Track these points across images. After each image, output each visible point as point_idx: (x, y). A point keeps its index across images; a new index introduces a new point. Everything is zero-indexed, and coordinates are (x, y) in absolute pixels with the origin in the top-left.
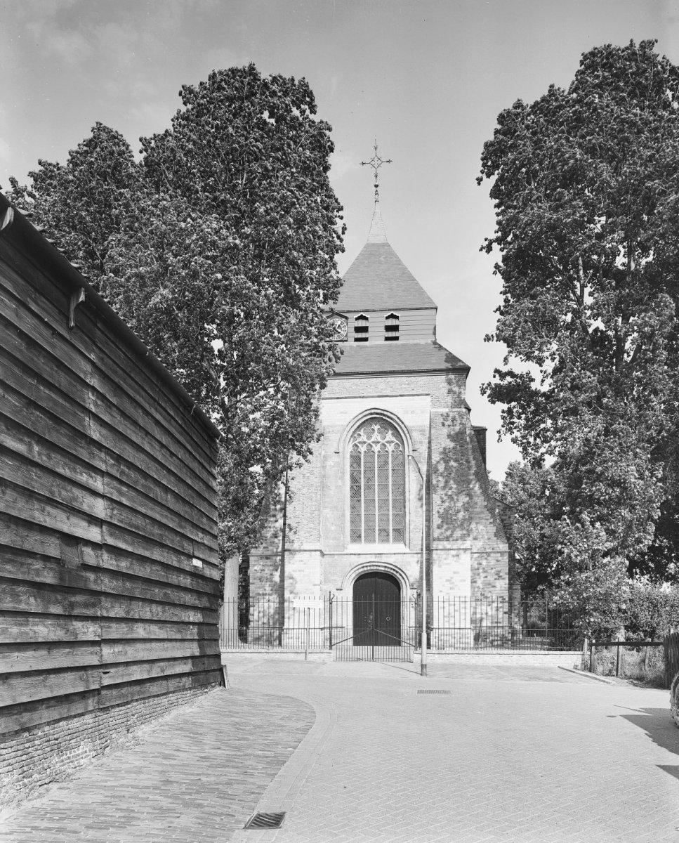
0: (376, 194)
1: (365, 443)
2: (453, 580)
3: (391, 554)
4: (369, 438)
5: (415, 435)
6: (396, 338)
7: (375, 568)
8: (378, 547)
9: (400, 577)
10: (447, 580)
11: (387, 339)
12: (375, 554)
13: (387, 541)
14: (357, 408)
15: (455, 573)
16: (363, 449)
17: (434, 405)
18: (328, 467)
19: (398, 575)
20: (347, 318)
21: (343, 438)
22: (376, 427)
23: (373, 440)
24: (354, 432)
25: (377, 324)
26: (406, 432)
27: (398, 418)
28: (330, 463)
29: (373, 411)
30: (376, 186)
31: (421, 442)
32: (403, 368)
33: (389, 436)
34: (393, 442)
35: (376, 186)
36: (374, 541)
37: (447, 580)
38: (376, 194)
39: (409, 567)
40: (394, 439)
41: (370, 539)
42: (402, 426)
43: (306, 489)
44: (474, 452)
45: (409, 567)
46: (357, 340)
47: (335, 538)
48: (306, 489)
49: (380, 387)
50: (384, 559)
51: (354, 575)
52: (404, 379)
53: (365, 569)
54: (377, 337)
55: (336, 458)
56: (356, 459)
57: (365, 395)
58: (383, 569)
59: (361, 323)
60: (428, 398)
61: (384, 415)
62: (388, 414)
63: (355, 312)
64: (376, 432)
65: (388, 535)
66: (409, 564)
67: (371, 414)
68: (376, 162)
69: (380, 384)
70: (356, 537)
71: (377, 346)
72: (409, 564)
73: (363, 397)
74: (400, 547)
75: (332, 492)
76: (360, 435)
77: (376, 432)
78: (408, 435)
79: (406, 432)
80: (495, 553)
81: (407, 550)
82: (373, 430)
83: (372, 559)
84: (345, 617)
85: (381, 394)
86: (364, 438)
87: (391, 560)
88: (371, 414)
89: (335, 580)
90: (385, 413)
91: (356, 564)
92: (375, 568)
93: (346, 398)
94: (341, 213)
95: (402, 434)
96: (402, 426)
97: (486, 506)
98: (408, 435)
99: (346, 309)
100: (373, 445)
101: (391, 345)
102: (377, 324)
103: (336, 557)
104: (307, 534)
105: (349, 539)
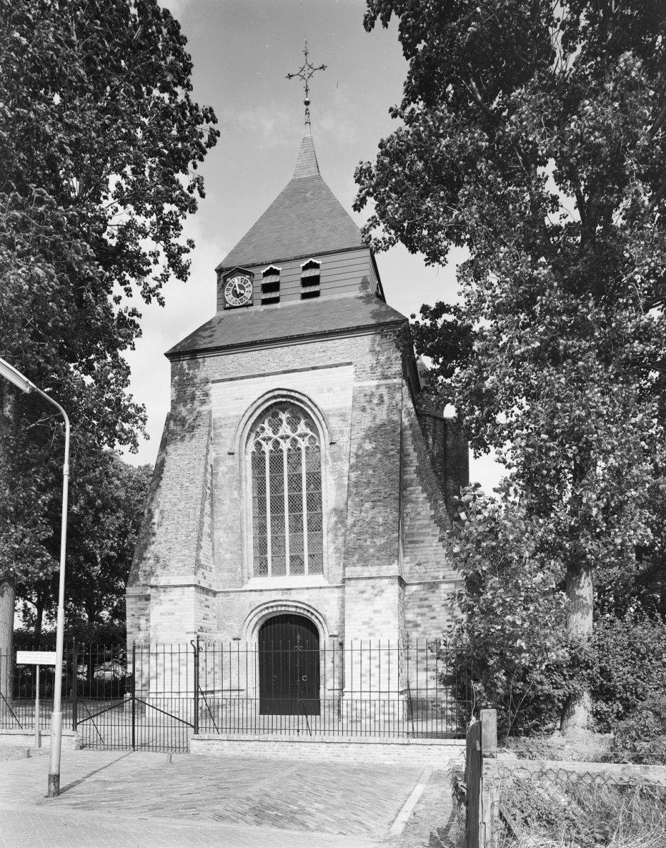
0: (307, 113)
1: (270, 439)
2: (373, 623)
3: (302, 589)
4: (275, 432)
5: (334, 422)
6: (316, 294)
7: (283, 609)
8: (289, 580)
9: (316, 621)
10: (364, 623)
11: (305, 296)
12: (282, 590)
13: (302, 572)
14: (252, 392)
15: (375, 612)
16: (267, 448)
17: (358, 378)
18: (220, 474)
19: (313, 618)
20: (249, 273)
21: (239, 433)
22: (284, 416)
23: (298, 432)
24: (255, 424)
25: (291, 277)
26: (321, 419)
27: (310, 400)
28: (222, 469)
29: (276, 393)
30: (307, 103)
31: (341, 432)
32: (316, 329)
33: (302, 428)
34: (306, 435)
35: (307, 103)
36: (285, 573)
37: (364, 623)
38: (307, 113)
39: (326, 607)
40: (308, 431)
41: (279, 571)
42: (316, 410)
43: (183, 503)
44: (415, 440)
45: (326, 607)
46: (265, 302)
47: (230, 570)
48: (183, 503)
49: (287, 359)
50: (294, 596)
51: (256, 619)
52: (318, 346)
53: (270, 610)
54: (291, 299)
55: (230, 462)
56: (258, 462)
57: (267, 371)
58: (294, 609)
59: (272, 279)
60: (351, 368)
61: (293, 398)
62: (297, 395)
63: (296, 259)
64: (285, 423)
65: (302, 563)
66: (327, 601)
67: (275, 397)
68: (307, 72)
69: (286, 355)
70: (262, 569)
71: (290, 308)
72: (327, 601)
73: (263, 375)
74: (318, 579)
75: (225, 508)
76: (263, 429)
77: (285, 423)
78: (323, 422)
79: (321, 419)
80: (446, 583)
81: (325, 584)
82: (281, 420)
83: (275, 596)
84: (248, 678)
85: (286, 369)
86: (268, 432)
87: (304, 597)
88: (275, 397)
89: (231, 626)
90: (293, 394)
91: (257, 605)
92: (283, 609)
93: (242, 378)
94: (198, 162)
95: (317, 422)
96: (316, 410)
97: (432, 517)
98: (323, 422)
99: (249, 262)
100: (300, 439)
101: (308, 304)
102: (291, 277)
103: (232, 594)
104: (180, 564)
105: (252, 571)
